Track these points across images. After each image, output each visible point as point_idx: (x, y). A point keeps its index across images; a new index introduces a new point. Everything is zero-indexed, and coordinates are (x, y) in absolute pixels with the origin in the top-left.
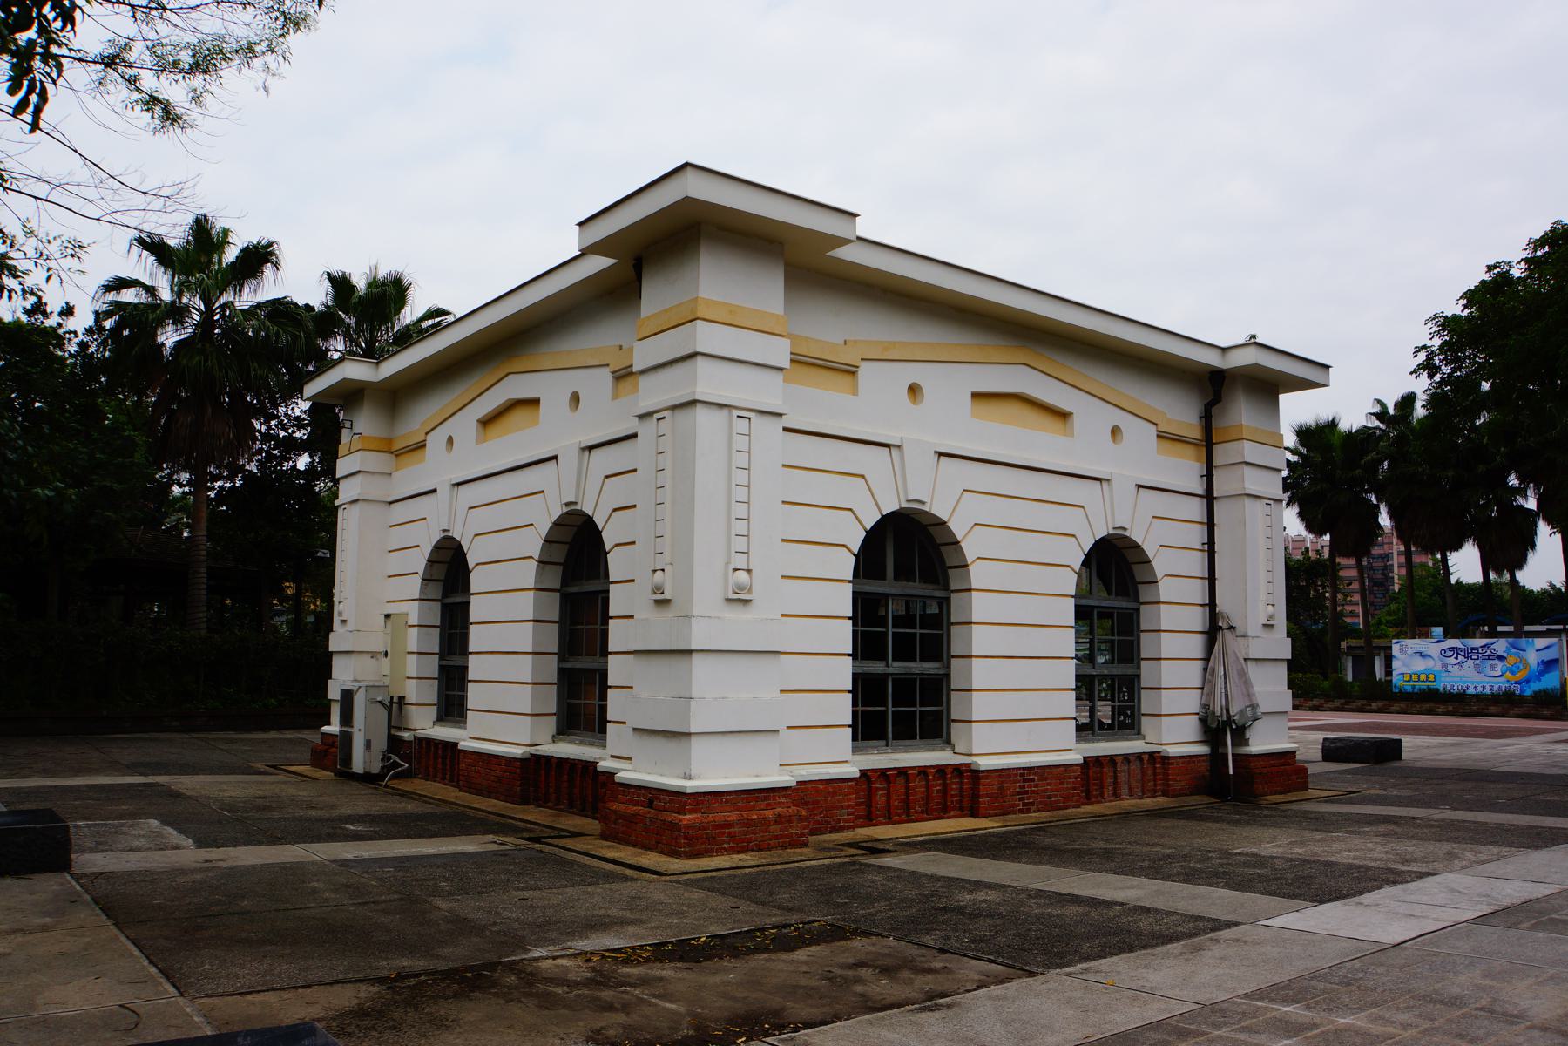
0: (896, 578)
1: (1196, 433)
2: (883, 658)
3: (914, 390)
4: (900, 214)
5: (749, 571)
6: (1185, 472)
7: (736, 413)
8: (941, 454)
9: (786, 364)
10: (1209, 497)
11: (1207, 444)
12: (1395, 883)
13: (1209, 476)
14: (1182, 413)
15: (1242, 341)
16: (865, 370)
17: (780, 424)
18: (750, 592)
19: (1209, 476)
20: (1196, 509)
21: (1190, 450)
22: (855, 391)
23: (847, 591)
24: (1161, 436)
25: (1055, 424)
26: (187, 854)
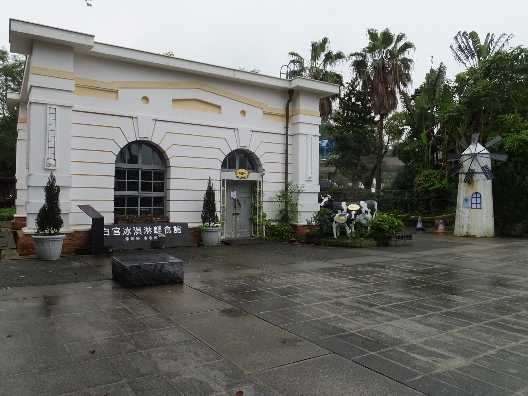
0: (143, 163)
1: (283, 112)
2: (137, 190)
3: (243, 112)
4: (111, 31)
5: (55, 160)
6: (278, 126)
7: (49, 106)
8: (253, 131)
9: (72, 88)
10: (287, 135)
11: (287, 117)
12: (319, 269)
13: (287, 128)
14: (277, 105)
15: (162, 54)
16: (120, 91)
17: (73, 109)
18: (55, 166)
19: (287, 128)
20: (281, 139)
21: (279, 118)
22: (220, 112)
23: (113, 167)
24: (264, 113)
25: (216, 110)
26: (440, 266)
